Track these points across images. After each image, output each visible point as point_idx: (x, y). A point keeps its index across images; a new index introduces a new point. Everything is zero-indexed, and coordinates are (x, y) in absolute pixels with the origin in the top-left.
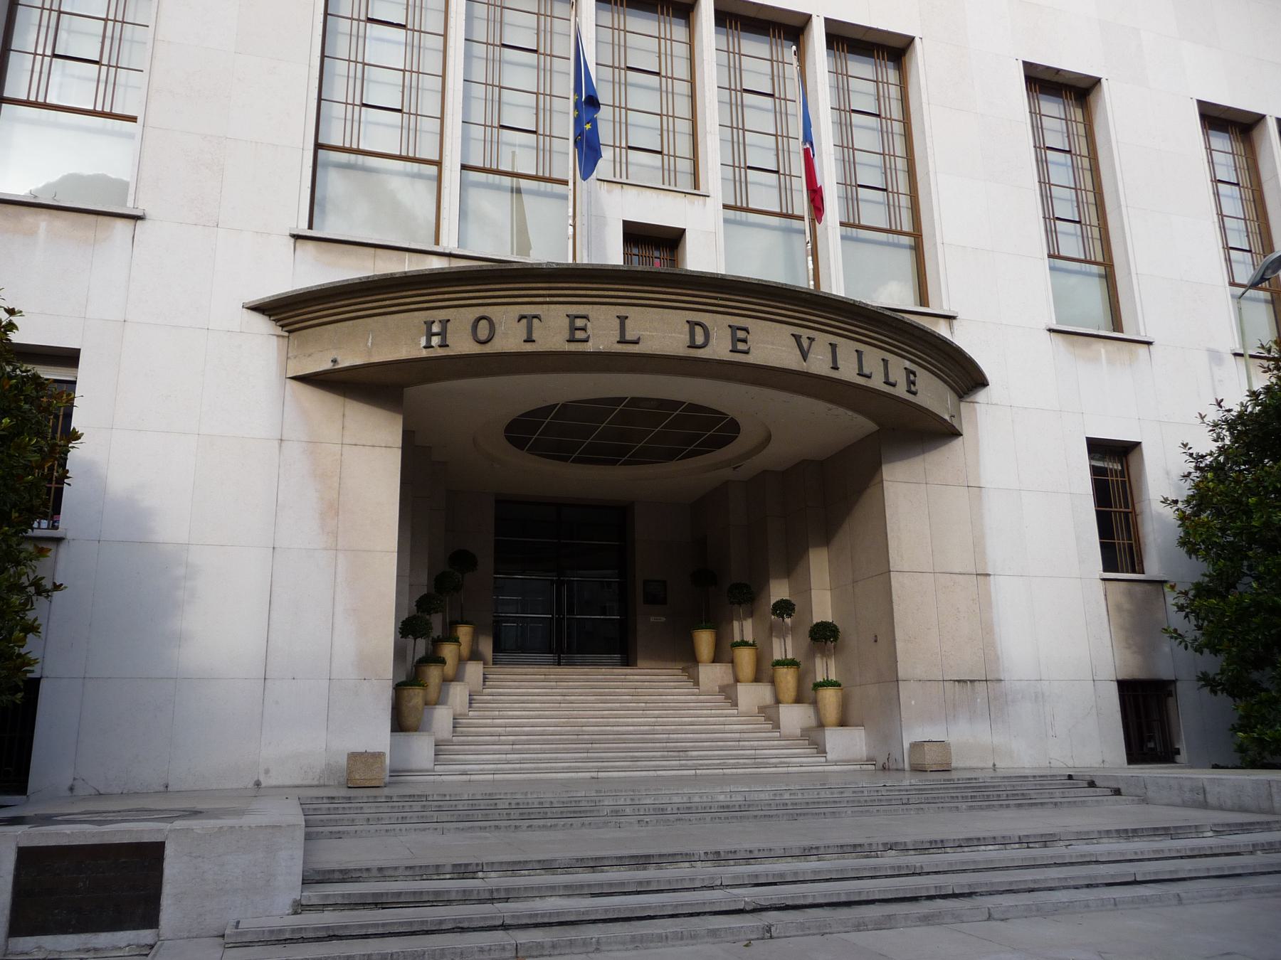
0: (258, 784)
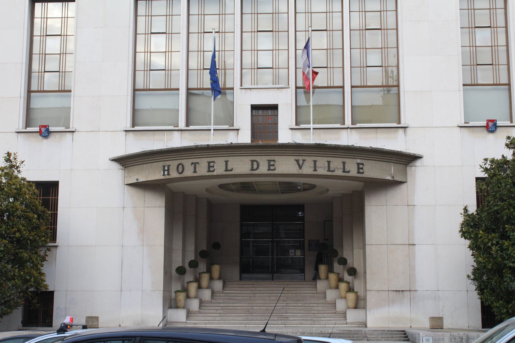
0: (120, 325)
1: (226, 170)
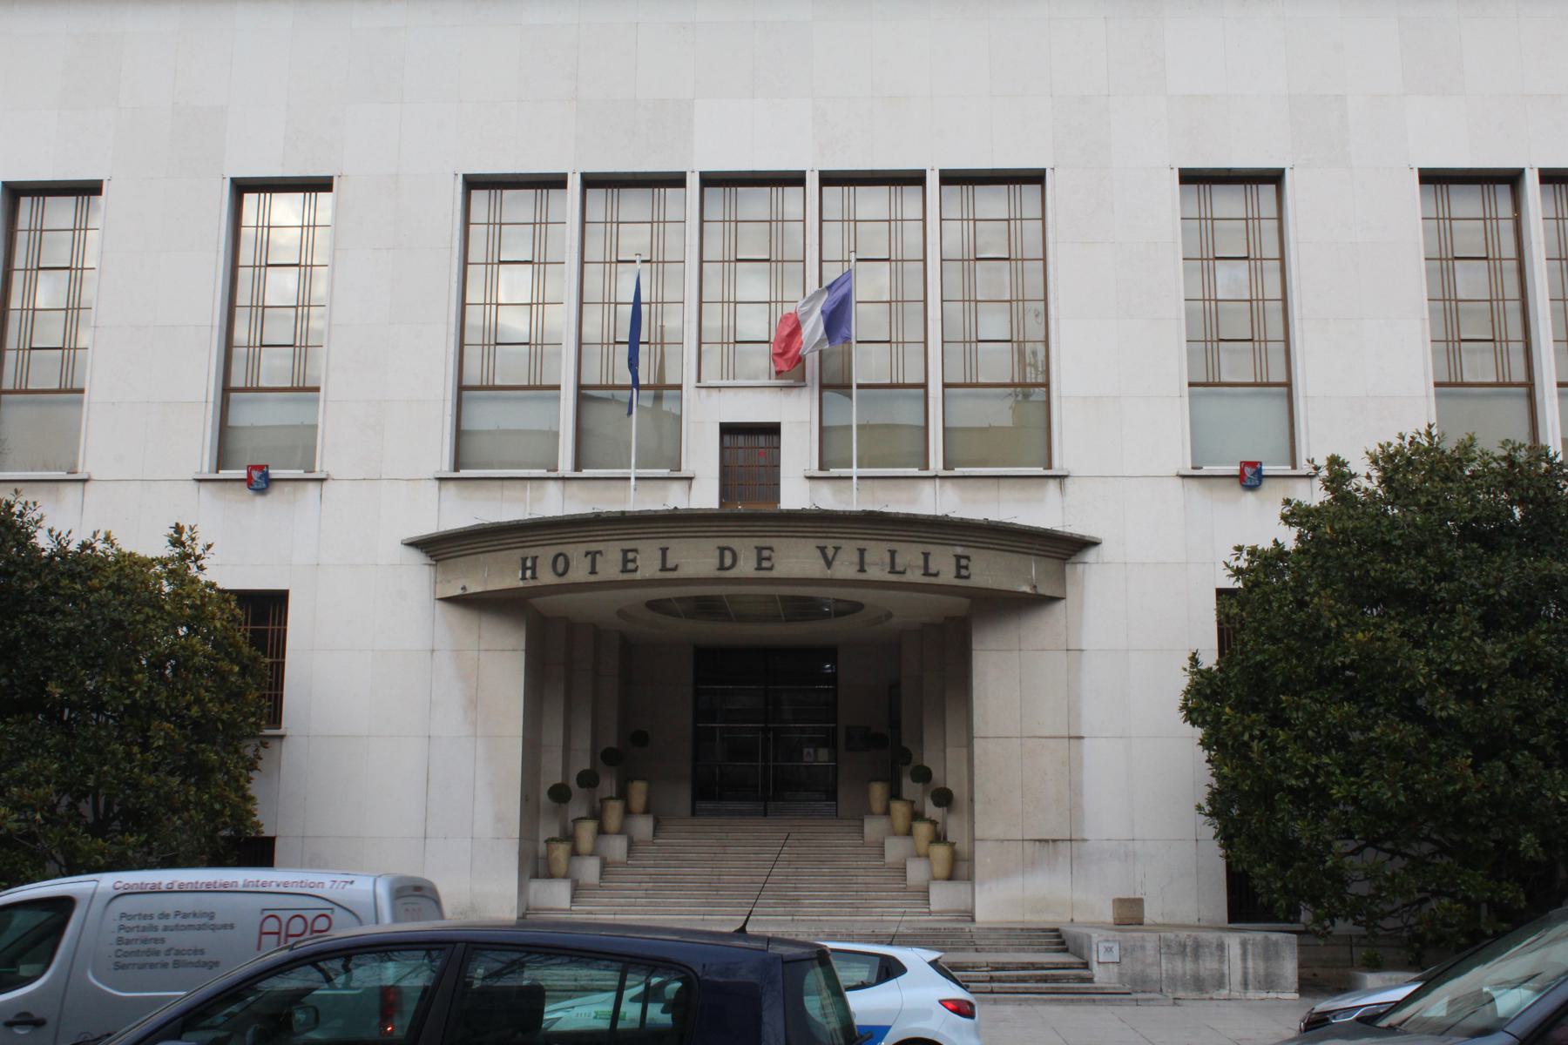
1: (664, 569)
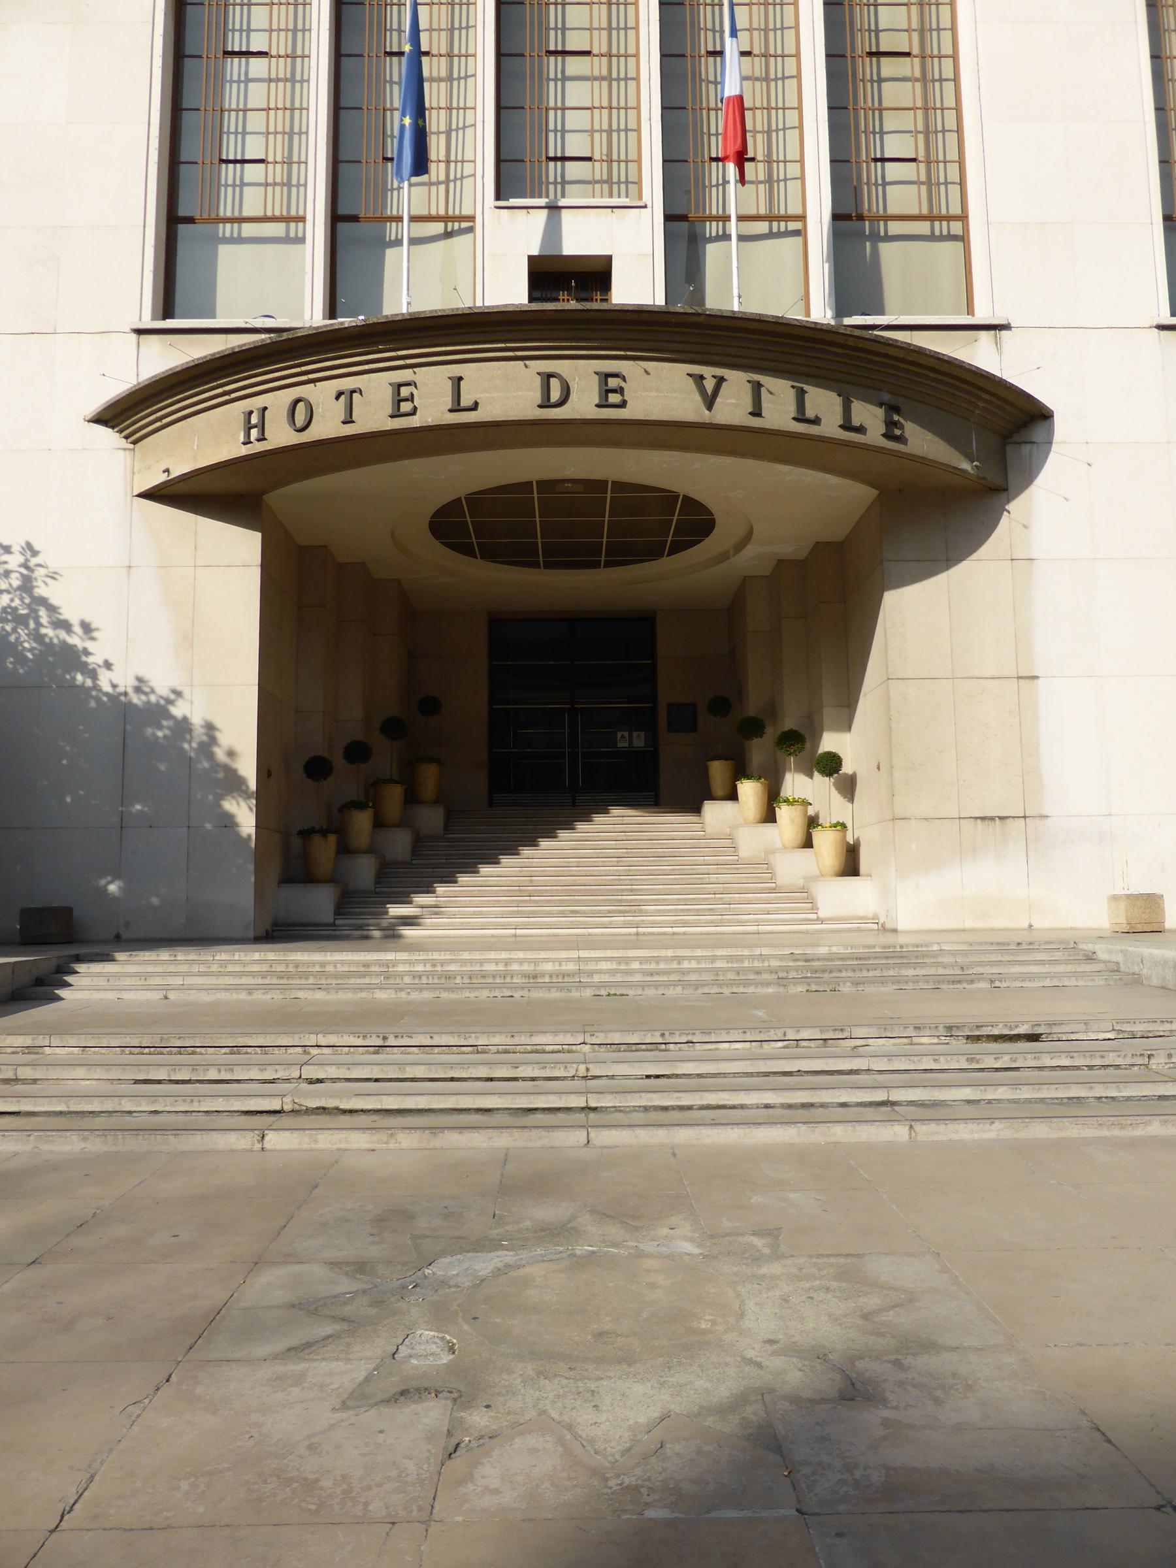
1: (456, 408)
